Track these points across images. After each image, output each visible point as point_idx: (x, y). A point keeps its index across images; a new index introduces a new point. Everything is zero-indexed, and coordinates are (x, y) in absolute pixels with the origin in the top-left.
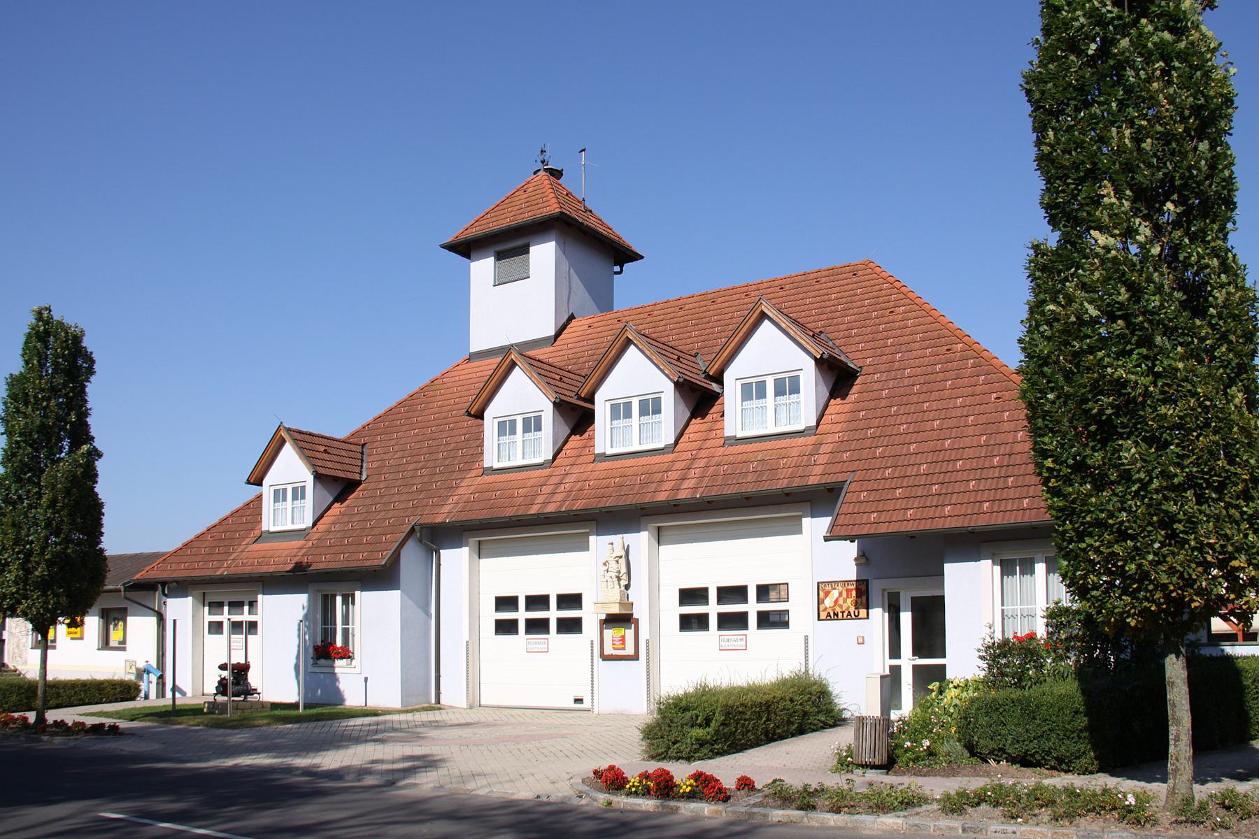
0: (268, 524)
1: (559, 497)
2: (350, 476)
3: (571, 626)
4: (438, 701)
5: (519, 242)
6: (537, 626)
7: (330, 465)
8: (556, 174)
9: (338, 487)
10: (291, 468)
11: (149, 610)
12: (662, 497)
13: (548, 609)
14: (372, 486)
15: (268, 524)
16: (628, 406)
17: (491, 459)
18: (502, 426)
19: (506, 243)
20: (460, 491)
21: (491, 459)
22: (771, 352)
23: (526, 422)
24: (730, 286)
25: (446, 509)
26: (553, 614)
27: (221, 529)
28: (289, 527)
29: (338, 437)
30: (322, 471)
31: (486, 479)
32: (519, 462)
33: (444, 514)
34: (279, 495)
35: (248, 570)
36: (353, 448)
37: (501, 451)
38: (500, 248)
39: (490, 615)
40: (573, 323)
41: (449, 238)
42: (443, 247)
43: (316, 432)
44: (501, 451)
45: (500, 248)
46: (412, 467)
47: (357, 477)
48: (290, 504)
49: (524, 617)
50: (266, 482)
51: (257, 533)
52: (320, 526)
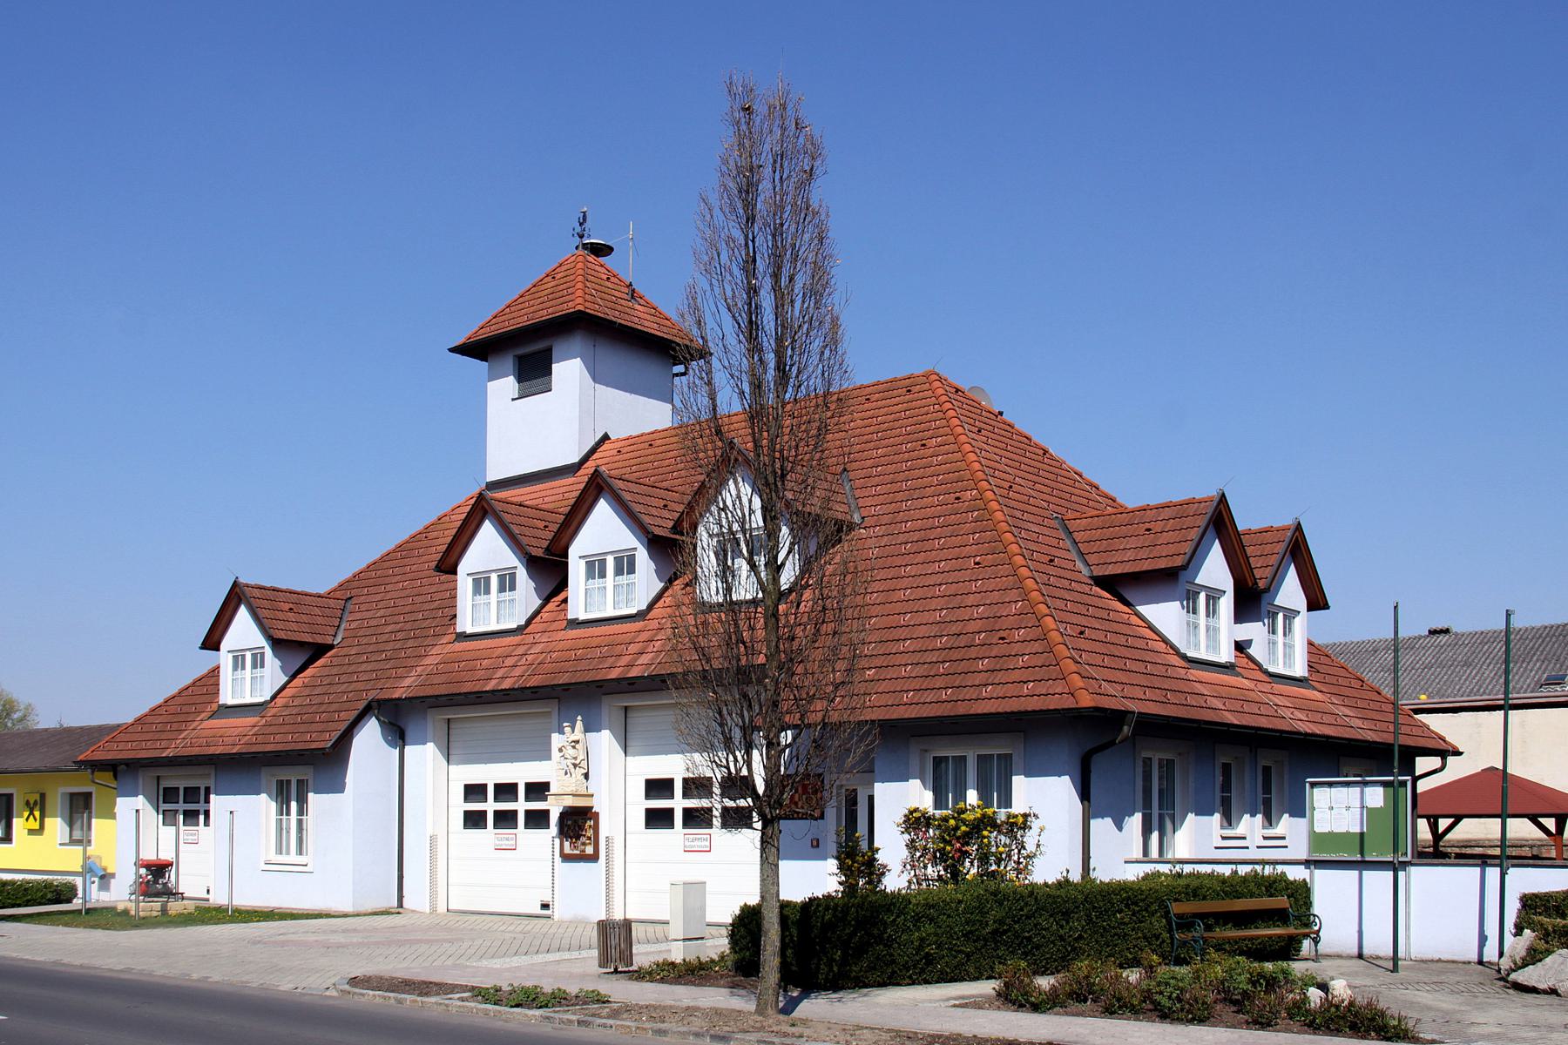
0: (227, 697)
1: (518, 671)
2: (319, 640)
3: (537, 819)
4: (400, 905)
5: (540, 346)
6: (505, 819)
7: (294, 627)
8: (600, 250)
9: (299, 650)
10: (244, 631)
11: (1500, 865)
12: (614, 674)
13: (516, 800)
14: (345, 651)
15: (227, 697)
16: (603, 563)
17: (466, 624)
18: (476, 582)
19: (524, 350)
20: (427, 661)
21: (466, 624)
22: (603, 530)
23: (618, 562)
24: (890, 377)
25: (407, 682)
26: (521, 806)
27: (179, 700)
28: (248, 700)
29: (322, 592)
30: (282, 635)
31: (459, 646)
32: (610, 612)
33: (405, 687)
34: (238, 662)
35: (196, 751)
36: (332, 603)
37: (478, 612)
38: (521, 351)
39: (460, 806)
40: (605, 446)
41: (459, 340)
42: (464, 350)
43: (268, 585)
44: (478, 612)
45: (521, 351)
46: (389, 628)
47: (329, 640)
48: (250, 676)
49: (489, 810)
50: (226, 644)
51: (215, 706)
52: (280, 701)
